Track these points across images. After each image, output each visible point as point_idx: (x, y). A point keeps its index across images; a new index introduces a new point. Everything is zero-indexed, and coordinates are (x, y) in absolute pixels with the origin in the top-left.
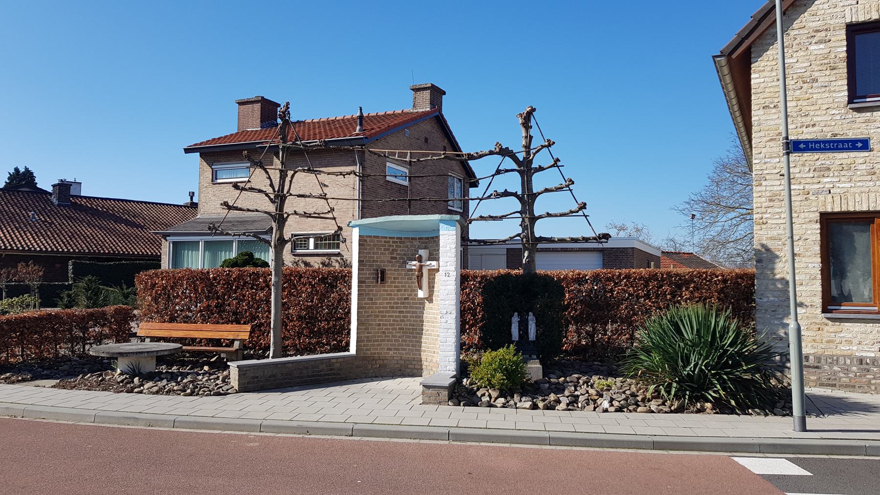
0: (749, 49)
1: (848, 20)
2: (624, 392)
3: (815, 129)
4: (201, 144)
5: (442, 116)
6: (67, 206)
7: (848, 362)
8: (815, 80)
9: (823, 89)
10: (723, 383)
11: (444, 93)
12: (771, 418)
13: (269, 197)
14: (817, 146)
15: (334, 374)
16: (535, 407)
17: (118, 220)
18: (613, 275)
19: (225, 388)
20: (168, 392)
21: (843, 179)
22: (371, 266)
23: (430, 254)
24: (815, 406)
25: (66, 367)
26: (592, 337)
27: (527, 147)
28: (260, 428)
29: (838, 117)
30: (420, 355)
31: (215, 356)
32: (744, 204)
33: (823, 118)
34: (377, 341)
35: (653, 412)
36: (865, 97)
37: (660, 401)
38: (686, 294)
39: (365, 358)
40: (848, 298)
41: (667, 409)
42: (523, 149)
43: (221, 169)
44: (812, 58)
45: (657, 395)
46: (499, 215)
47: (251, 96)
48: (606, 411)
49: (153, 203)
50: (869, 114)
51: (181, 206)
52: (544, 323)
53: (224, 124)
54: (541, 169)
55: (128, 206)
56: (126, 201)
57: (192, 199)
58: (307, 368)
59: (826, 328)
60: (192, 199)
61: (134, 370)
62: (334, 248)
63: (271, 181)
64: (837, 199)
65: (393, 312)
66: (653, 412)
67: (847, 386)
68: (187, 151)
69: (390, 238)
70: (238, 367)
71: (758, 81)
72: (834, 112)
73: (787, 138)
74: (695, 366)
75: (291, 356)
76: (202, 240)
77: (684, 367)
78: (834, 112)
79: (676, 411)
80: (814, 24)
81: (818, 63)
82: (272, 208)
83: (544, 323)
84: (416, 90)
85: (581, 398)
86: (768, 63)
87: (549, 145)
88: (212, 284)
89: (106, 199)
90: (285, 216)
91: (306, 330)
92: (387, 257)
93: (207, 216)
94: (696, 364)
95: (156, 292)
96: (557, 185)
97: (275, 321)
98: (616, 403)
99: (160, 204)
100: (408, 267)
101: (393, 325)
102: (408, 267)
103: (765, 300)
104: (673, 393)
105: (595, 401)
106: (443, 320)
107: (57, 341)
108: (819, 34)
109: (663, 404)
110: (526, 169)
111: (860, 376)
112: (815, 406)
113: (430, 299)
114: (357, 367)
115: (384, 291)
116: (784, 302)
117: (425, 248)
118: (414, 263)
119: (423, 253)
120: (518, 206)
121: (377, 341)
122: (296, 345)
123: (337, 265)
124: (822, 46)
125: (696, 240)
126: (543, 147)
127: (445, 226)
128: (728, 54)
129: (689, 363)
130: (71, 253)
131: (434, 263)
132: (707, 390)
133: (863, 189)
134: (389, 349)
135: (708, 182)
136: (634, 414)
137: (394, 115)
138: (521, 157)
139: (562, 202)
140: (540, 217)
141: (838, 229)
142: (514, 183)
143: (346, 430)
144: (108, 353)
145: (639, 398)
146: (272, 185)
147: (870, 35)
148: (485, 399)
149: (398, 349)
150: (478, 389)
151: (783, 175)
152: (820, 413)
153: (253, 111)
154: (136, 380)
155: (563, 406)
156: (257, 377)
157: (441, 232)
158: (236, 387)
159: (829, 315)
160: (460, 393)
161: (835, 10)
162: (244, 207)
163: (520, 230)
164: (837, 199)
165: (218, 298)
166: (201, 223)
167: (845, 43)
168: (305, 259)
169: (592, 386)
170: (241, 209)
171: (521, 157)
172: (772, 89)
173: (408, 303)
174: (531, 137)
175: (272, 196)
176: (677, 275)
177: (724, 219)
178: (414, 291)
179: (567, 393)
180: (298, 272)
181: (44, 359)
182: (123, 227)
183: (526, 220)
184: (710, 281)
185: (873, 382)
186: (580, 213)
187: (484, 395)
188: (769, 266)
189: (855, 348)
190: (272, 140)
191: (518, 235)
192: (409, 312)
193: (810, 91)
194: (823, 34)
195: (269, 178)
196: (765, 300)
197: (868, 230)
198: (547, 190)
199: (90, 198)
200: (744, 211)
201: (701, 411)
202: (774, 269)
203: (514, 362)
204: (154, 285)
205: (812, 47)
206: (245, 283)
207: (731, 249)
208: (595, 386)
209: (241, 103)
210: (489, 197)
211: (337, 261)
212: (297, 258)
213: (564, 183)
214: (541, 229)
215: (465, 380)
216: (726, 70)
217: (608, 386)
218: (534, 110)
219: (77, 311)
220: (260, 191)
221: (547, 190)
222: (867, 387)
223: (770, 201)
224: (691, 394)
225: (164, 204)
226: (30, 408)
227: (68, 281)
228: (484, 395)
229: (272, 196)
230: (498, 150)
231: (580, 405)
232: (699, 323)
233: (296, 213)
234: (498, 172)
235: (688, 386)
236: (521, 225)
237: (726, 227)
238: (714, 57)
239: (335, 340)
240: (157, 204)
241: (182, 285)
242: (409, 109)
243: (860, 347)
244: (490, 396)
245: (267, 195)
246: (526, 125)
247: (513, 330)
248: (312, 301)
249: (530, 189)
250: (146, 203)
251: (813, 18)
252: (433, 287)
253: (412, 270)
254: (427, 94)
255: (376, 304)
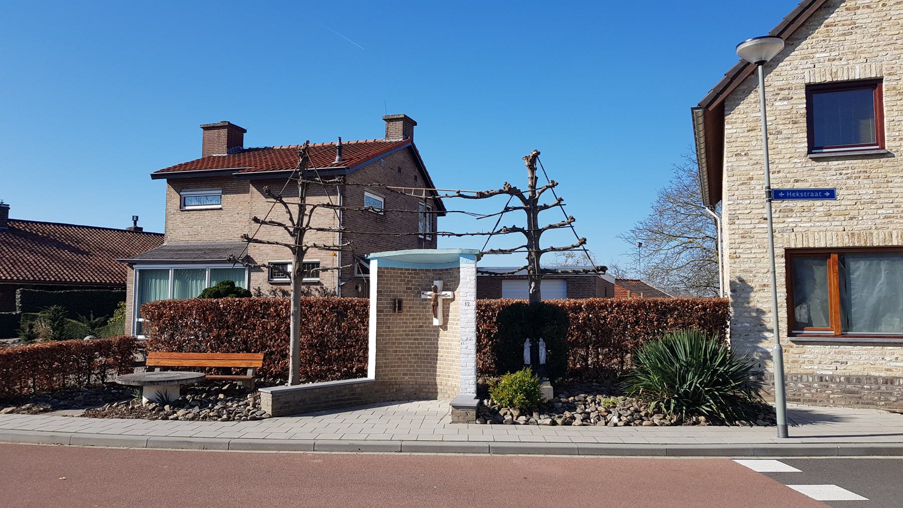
0: (723, 102)
1: (807, 81)
2: (628, 409)
3: (780, 175)
4: (169, 169)
5: (414, 146)
6: (4, 230)
7: (811, 379)
8: (780, 133)
9: (787, 141)
10: (714, 398)
11: (415, 124)
12: (755, 428)
13: (288, 230)
14: (794, 194)
15: (356, 399)
16: (554, 423)
17: (61, 246)
18: (606, 304)
19: (258, 413)
20: (204, 418)
21: (804, 219)
22: (388, 296)
23: (444, 285)
24: (795, 418)
25: (81, 397)
26: (586, 360)
27: (533, 187)
28: (314, 447)
29: (800, 165)
30: (435, 379)
31: (225, 384)
32: (686, 232)
33: (787, 166)
34: (394, 366)
35: (656, 425)
36: (822, 148)
37: (661, 416)
38: (671, 321)
39: (383, 383)
40: (809, 324)
41: (668, 423)
42: (529, 189)
43: (191, 196)
44: (777, 113)
45: (658, 410)
46: (508, 248)
47: (217, 121)
48: (616, 425)
49: (95, 228)
50: (825, 163)
51: (125, 231)
52: (553, 346)
53: (189, 150)
54: (546, 207)
55: (70, 231)
56: (67, 225)
57: (135, 223)
58: (332, 393)
59: (791, 350)
60: (135, 223)
61: (162, 397)
62: (313, 277)
63: (291, 215)
64: (799, 237)
65: (409, 339)
66: (656, 425)
67: (809, 401)
68: (154, 177)
69: (406, 270)
70: (272, 393)
71: (731, 131)
72: (796, 160)
73: (769, 187)
74: (691, 385)
75: (304, 383)
76: (171, 269)
77: (681, 386)
78: (796, 160)
79: (675, 424)
80: (779, 83)
81: (782, 117)
82: (291, 241)
83: (553, 346)
84: (389, 120)
85: (592, 415)
86: (740, 116)
87: (553, 186)
88: (222, 315)
89: (45, 223)
90: (304, 248)
91: (324, 356)
92: (403, 287)
93: (174, 244)
94: (693, 381)
95: (164, 323)
96: (560, 222)
97: (294, 349)
98: (624, 419)
99: (103, 229)
100: (423, 297)
101: (409, 351)
102: (423, 297)
103: (739, 325)
104: (672, 406)
105: (605, 417)
106: (464, 346)
107: (65, 373)
108: (783, 92)
109: (664, 418)
110: (532, 207)
111: (821, 392)
112: (795, 418)
113: (444, 326)
114: (376, 392)
115: (400, 319)
116: (758, 327)
117: (439, 279)
118: (429, 293)
119: (437, 283)
120: (525, 241)
121: (394, 366)
122: (307, 372)
123: (317, 294)
124: (785, 103)
125: (642, 266)
126: (548, 187)
127: (465, 260)
128: (704, 106)
129: (685, 382)
130: (15, 281)
131: (449, 293)
132: (700, 405)
133: (821, 228)
134: (406, 374)
135: (652, 211)
136: (640, 427)
137: (366, 145)
138: (527, 196)
139: (565, 238)
140: (545, 251)
141: (800, 262)
142: (520, 219)
143: (397, 446)
144: (139, 382)
145: (643, 414)
146: (291, 219)
147: (824, 95)
148: (508, 417)
149: (413, 374)
150: (499, 409)
151: (766, 219)
152: (794, 424)
153: (219, 136)
154: (167, 407)
155: (578, 421)
156: (288, 402)
157: (461, 265)
158: (269, 411)
159: (794, 339)
160: (486, 414)
161: (796, 72)
162: (265, 239)
163: (526, 263)
164: (799, 237)
165: (228, 327)
166: (169, 250)
167: (805, 101)
168: (283, 287)
169: (599, 404)
170: (261, 242)
171: (527, 196)
172: (743, 139)
173: (423, 331)
174: (536, 178)
175: (292, 230)
176: (662, 303)
177: (666, 247)
178: (428, 319)
179: (578, 410)
180: (309, 302)
181: (54, 390)
182: (66, 254)
183: (533, 253)
184: (692, 309)
185: (831, 396)
186: (581, 247)
187: (506, 414)
188: (743, 296)
189: (816, 367)
190: (225, 167)
191: (526, 267)
192: (424, 339)
193: (775, 142)
194: (786, 92)
195: (289, 212)
196: (739, 325)
197: (824, 265)
198: (551, 227)
199: (28, 222)
200: (686, 240)
201: (697, 423)
202: (749, 298)
203: (533, 384)
204: (161, 316)
205: (777, 104)
206: (256, 312)
207: (674, 277)
208: (602, 403)
209: (206, 128)
210: (498, 232)
211: (317, 289)
212: (275, 287)
213: (566, 220)
214: (547, 261)
215: (485, 401)
216: (701, 120)
217: (614, 403)
218: (539, 153)
219: (39, 344)
220: (280, 225)
221: (551, 227)
222: (826, 401)
223: (743, 237)
224: (687, 409)
225: (107, 229)
226: (76, 435)
227: (15, 310)
228: (506, 414)
229: (292, 230)
230: (507, 189)
231: (592, 421)
232: (691, 347)
233: (315, 246)
234: (507, 209)
235: (686, 402)
236: (528, 258)
237: (669, 255)
238: (693, 109)
239: (346, 367)
240: (99, 228)
241: (191, 315)
242: (381, 138)
243: (820, 366)
244: (511, 414)
245: (286, 228)
246: (532, 168)
247: (525, 354)
248: (323, 330)
249: (536, 225)
250: (87, 227)
251: (777, 78)
252: (448, 316)
253: (426, 300)
254: (400, 125)
255: (393, 331)
